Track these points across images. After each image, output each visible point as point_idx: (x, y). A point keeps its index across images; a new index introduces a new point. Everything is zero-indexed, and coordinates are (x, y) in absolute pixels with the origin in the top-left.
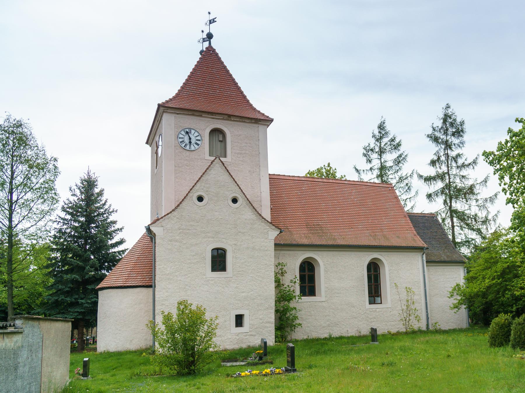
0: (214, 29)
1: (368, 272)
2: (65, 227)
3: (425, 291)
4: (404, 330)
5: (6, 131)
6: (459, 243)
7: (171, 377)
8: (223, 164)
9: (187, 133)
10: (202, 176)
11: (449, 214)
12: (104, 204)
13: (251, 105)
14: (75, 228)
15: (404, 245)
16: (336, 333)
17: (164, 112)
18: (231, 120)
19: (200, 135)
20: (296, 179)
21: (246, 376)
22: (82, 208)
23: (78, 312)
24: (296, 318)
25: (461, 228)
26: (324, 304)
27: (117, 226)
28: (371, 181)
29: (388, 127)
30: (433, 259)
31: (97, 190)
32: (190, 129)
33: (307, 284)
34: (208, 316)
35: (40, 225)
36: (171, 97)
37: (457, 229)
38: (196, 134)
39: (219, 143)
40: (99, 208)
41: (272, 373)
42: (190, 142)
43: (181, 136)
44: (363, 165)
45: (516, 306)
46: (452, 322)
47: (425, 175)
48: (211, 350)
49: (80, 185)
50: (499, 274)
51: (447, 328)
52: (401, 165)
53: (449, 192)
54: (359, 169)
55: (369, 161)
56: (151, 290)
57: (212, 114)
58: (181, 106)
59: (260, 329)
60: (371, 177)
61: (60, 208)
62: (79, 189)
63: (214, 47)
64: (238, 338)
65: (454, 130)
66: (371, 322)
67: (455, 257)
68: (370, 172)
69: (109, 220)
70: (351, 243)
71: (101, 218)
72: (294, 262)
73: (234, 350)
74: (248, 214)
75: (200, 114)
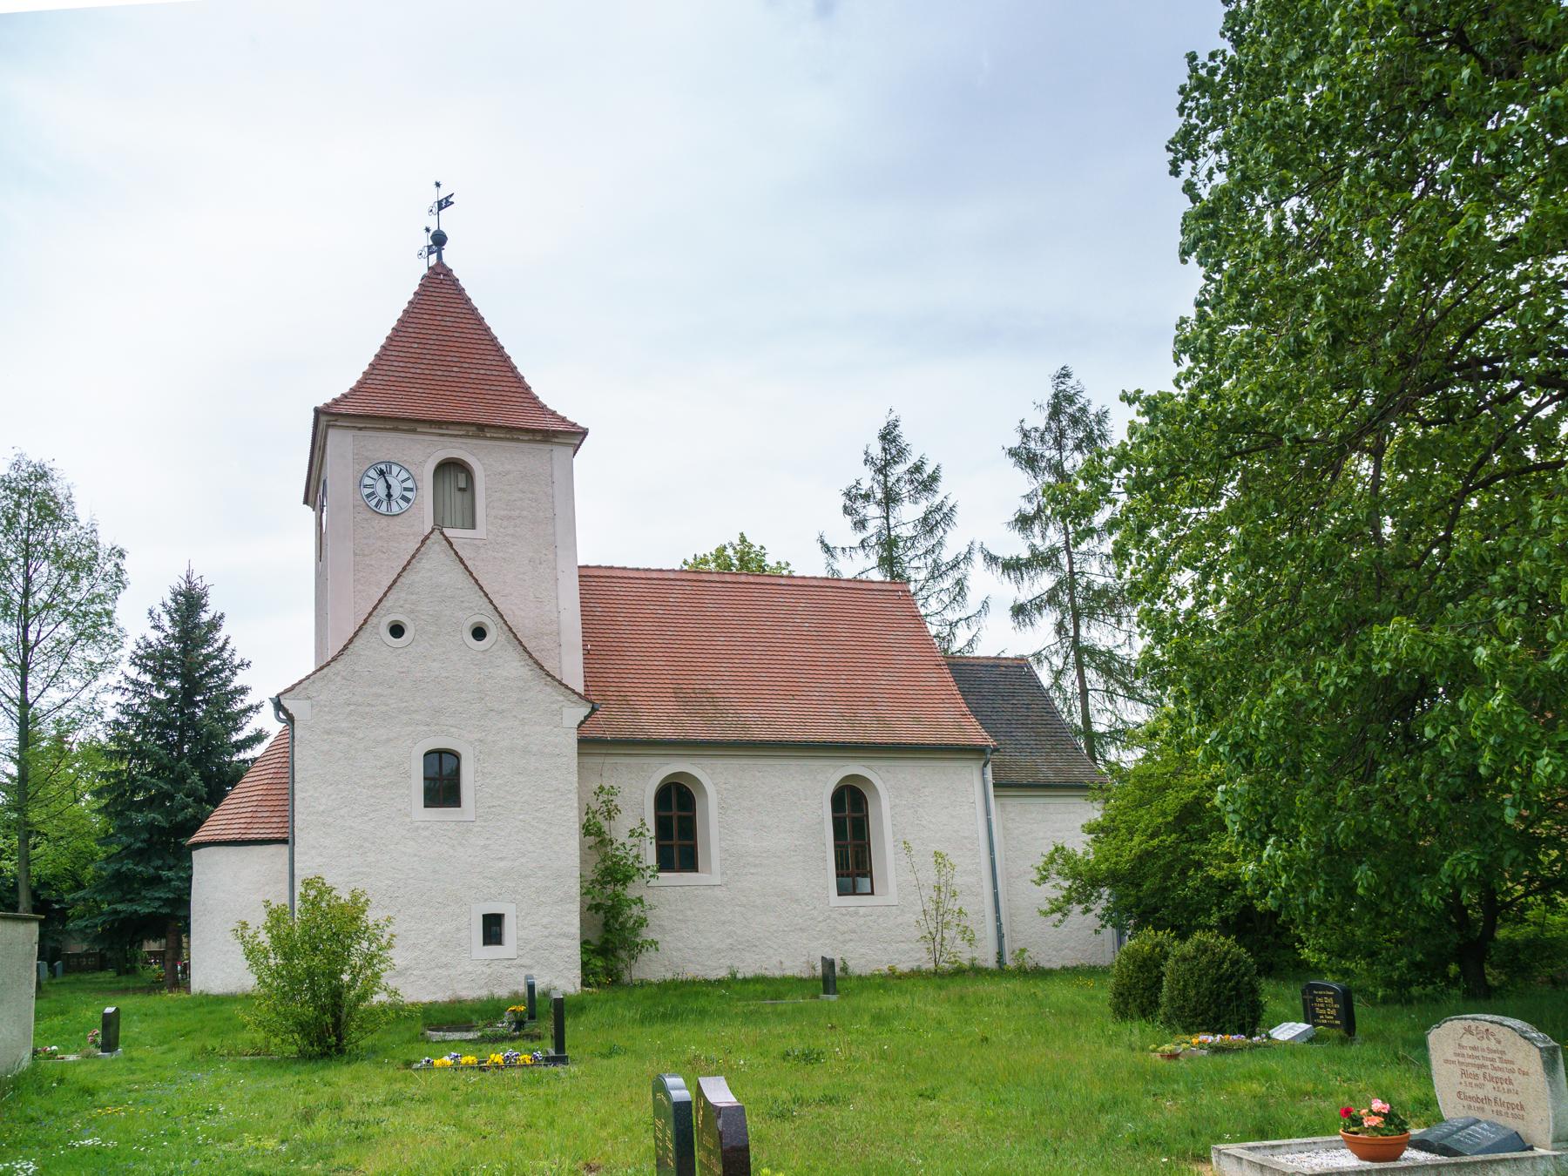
0: (448, 221)
1: (834, 810)
2: (137, 701)
3: (981, 862)
4: (931, 966)
5: (13, 490)
6: (1103, 735)
7: (284, 1063)
8: (451, 544)
9: (382, 473)
10: (399, 575)
11: (1071, 659)
12: (222, 649)
13: (535, 398)
14: (155, 703)
15: (930, 739)
16: (747, 970)
17: (328, 426)
18: (486, 438)
19: (411, 477)
20: (654, 575)
21: (444, 1068)
22: (172, 658)
23: (159, 899)
24: (641, 922)
25: (1111, 694)
26: (717, 892)
27: (249, 700)
28: (864, 577)
29: (906, 434)
30: (1014, 777)
31: (205, 617)
32: (389, 464)
33: (675, 841)
34: (371, 917)
35: (96, 697)
36: (346, 390)
37: (1095, 700)
38: (404, 475)
39: (459, 494)
40: (209, 657)
41: (509, 1063)
42: (389, 496)
43: (367, 481)
44: (842, 533)
45: (1220, 909)
46: (1072, 949)
47: (1005, 553)
48: (376, 999)
49: (170, 603)
50: (1170, 819)
51: (1056, 964)
52: (939, 532)
53: (1072, 599)
54: (831, 545)
55: (861, 524)
56: (284, 849)
57: (439, 425)
58: (368, 411)
59: (549, 955)
60: (861, 565)
61: (126, 659)
62: (169, 613)
63: (449, 265)
64: (489, 971)
65: (1081, 435)
66: (844, 942)
67: (1078, 773)
68: (861, 552)
69: (231, 687)
70: (787, 738)
71: (213, 682)
72: (637, 789)
73: (479, 1000)
74: (513, 667)
75: (413, 425)
